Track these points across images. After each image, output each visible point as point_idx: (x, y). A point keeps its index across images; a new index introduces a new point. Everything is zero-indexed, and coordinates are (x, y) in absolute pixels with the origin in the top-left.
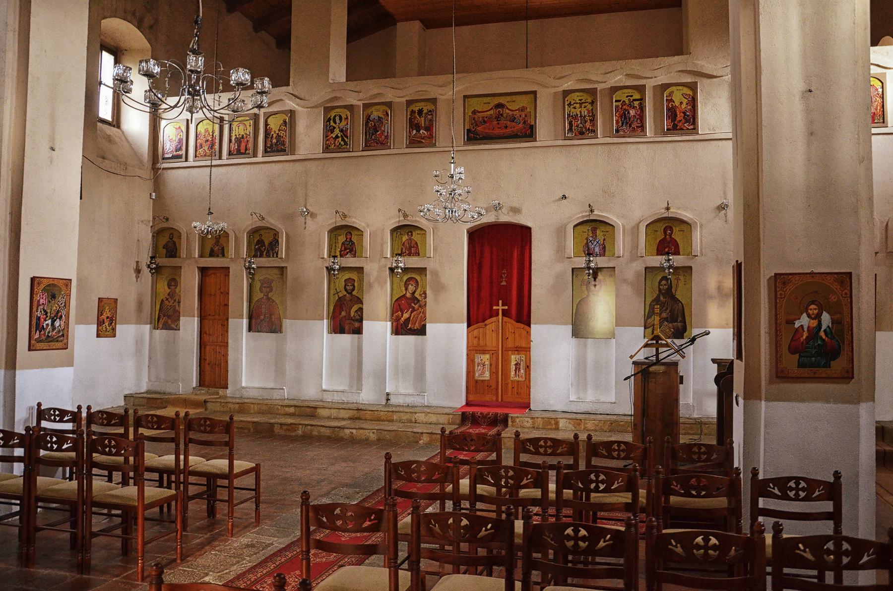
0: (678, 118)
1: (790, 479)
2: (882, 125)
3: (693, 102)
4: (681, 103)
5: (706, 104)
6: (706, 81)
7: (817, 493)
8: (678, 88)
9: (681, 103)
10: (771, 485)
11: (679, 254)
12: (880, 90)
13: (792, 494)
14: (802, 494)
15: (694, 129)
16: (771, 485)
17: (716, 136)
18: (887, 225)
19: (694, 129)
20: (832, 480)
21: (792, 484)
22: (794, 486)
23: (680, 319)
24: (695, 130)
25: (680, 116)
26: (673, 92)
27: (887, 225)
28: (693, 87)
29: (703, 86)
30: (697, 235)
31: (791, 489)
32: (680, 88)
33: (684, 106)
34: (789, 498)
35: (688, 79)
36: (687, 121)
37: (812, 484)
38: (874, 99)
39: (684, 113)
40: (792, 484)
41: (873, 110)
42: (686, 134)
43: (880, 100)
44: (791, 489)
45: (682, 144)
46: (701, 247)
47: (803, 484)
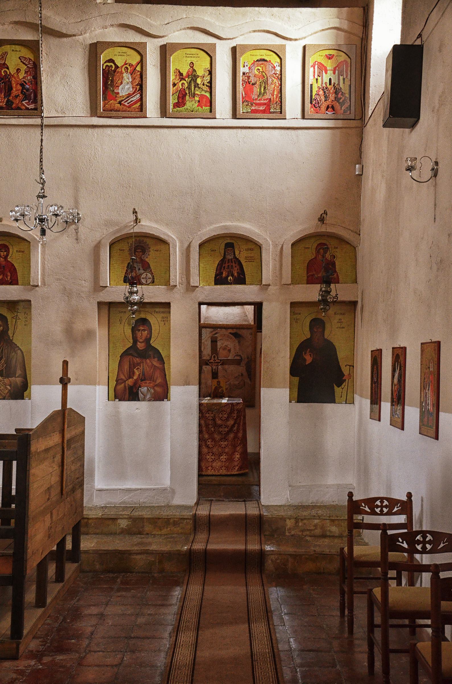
0: (14, 92)
1: (376, 499)
2: (279, 116)
3: (35, 69)
4: (18, 70)
5: (53, 75)
6: (54, 41)
7: (396, 509)
8: (13, 47)
9: (18, 70)
10: (363, 504)
11: (17, 284)
12: (278, 68)
13: (378, 510)
14: (385, 510)
15: (36, 109)
16: (363, 504)
17: (66, 121)
18: (282, 247)
19: (36, 109)
20: (405, 498)
21: (378, 503)
22: (379, 504)
23: (19, 372)
24: (37, 110)
25: (16, 90)
26: (6, 53)
27: (282, 247)
28: (34, 47)
29: (48, 48)
30: (38, 258)
31: (377, 507)
32: (18, 48)
33: (22, 75)
34: (376, 514)
35: (28, 36)
36: (26, 97)
37: (393, 502)
38: (270, 81)
39: (22, 85)
40: (378, 503)
41: (268, 96)
42: (24, 116)
43: (277, 82)
44: (377, 507)
45: (19, 130)
46: (43, 275)
47: (386, 503)
